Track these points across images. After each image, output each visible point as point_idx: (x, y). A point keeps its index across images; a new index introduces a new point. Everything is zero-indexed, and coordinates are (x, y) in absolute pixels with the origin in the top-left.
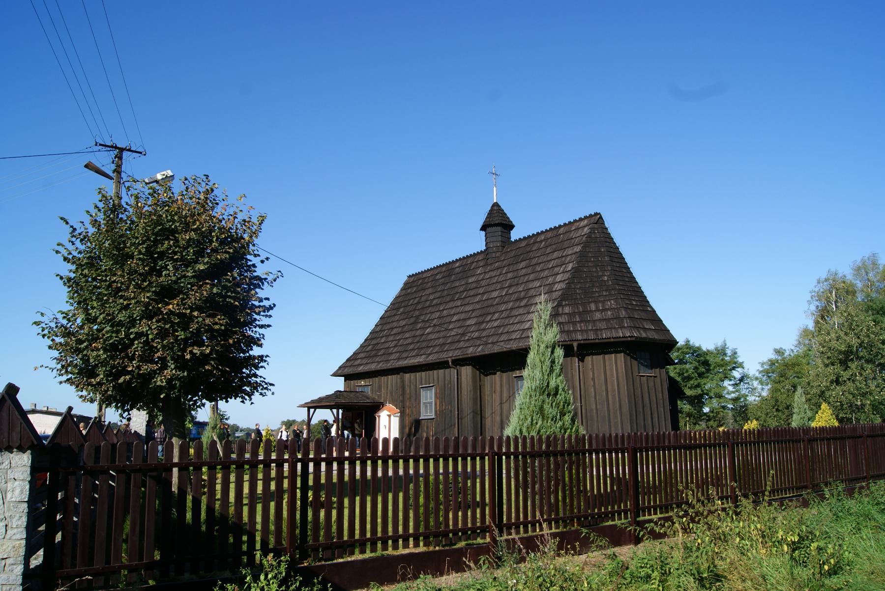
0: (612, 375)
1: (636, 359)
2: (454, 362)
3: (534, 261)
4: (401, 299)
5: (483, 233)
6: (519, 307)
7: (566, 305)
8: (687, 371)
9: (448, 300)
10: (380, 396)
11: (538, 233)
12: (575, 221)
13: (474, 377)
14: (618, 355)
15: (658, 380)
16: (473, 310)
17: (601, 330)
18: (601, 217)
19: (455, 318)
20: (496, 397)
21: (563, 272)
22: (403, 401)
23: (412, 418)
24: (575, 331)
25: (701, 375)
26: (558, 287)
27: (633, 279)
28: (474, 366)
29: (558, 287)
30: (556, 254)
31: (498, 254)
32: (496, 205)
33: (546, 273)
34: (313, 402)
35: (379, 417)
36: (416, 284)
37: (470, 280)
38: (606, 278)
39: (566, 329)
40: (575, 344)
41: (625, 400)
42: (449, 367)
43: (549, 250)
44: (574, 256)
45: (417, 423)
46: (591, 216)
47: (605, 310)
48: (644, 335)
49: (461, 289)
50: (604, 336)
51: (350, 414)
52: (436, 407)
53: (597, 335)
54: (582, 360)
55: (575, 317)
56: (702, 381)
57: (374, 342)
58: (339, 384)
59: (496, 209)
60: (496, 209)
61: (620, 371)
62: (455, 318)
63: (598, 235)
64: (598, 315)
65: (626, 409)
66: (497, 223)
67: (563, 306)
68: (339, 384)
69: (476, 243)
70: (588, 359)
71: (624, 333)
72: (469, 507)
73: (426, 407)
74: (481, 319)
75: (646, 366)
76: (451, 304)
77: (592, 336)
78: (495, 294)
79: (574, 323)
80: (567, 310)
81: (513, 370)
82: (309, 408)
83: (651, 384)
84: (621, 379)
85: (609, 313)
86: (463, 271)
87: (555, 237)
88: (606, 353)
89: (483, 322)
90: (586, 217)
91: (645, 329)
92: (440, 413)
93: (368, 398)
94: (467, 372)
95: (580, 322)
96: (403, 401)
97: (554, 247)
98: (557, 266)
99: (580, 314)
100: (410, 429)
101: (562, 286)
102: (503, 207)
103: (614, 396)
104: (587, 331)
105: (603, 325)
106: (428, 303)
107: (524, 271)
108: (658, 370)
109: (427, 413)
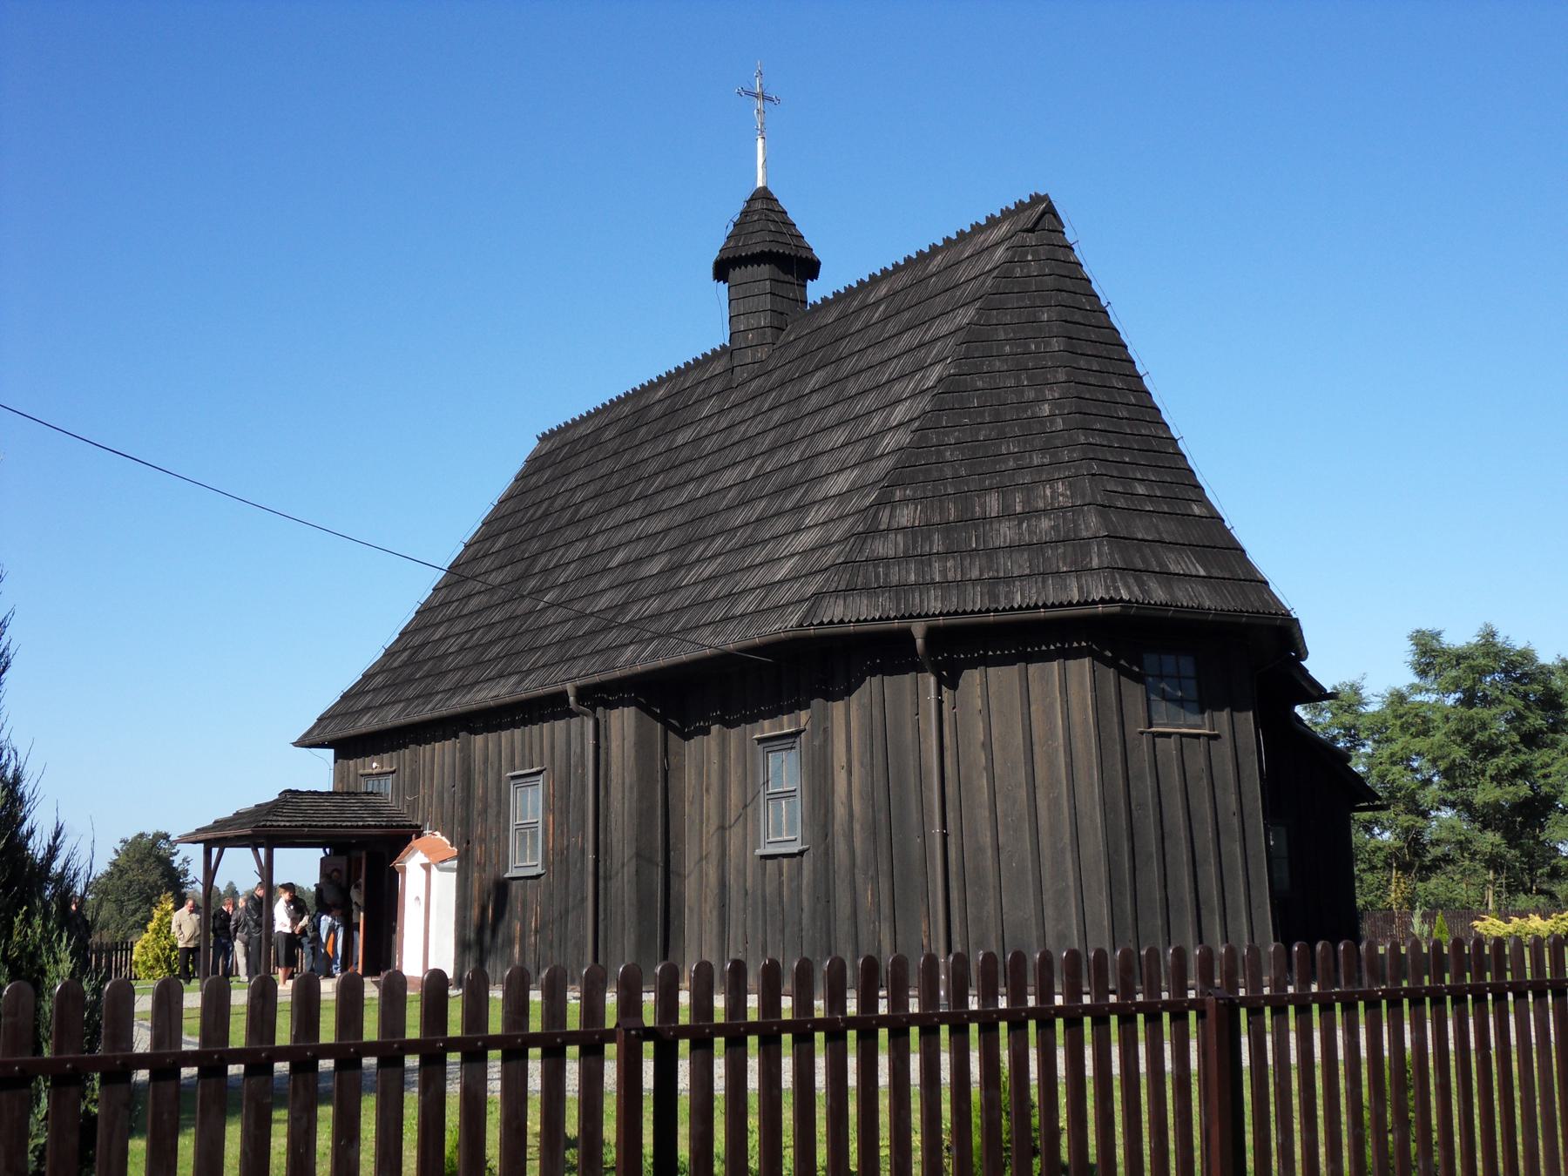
0: (1051, 732)
1: (1138, 678)
2: (584, 694)
3: (848, 367)
4: (510, 505)
5: (723, 287)
6: (778, 514)
7: (905, 501)
8: (1484, 726)
9: (615, 501)
10: (413, 807)
11: (873, 277)
12: (977, 229)
13: (642, 744)
14: (1072, 664)
15: (1224, 749)
16: (666, 531)
17: (1009, 579)
18: (1050, 210)
19: (620, 557)
20: (711, 801)
21: (913, 396)
22: (466, 822)
23: (490, 875)
24: (924, 585)
25: (1531, 740)
26: (889, 442)
27: (1148, 412)
28: (645, 709)
29: (889, 442)
30: (906, 340)
31: (762, 354)
32: (764, 195)
33: (869, 401)
34: (220, 824)
35: (404, 869)
36: (560, 455)
37: (680, 439)
38: (1046, 409)
39: (894, 579)
40: (918, 629)
41: (1093, 818)
42: (570, 714)
43: (891, 328)
44: (951, 341)
45: (501, 889)
46: (1021, 207)
47: (1031, 514)
48: (1159, 594)
49: (652, 467)
50: (1018, 600)
51: (342, 862)
52: (545, 842)
53: (994, 597)
54: (949, 680)
55: (929, 538)
56: (1539, 757)
57: (418, 640)
58: (317, 772)
59: (763, 209)
60: (763, 209)
61: (1076, 717)
62: (620, 557)
63: (1034, 269)
64: (1006, 532)
65: (1094, 844)
66: (765, 253)
67: (893, 504)
68: (317, 772)
69: (700, 322)
70: (972, 679)
71: (1091, 590)
72: (1035, 1152)
73: (524, 836)
74: (677, 557)
75: (1180, 702)
76: (619, 516)
77: (976, 600)
78: (729, 477)
79: (925, 559)
80: (906, 516)
81: (753, 719)
82: (208, 845)
83: (1197, 762)
84: (1078, 745)
85: (1045, 524)
86: (670, 413)
87: (914, 284)
88: (1029, 659)
89: (680, 566)
90: (1007, 214)
91: (1165, 575)
92: (558, 858)
93: (376, 812)
94: (623, 722)
95: (948, 553)
96: (466, 822)
97: (907, 315)
98: (901, 377)
99: (947, 527)
100: (484, 910)
101: (903, 438)
102: (784, 204)
103: (1054, 804)
104: (960, 584)
105: (1019, 564)
106: (568, 515)
107: (815, 400)
108: (1224, 715)
109: (525, 861)
